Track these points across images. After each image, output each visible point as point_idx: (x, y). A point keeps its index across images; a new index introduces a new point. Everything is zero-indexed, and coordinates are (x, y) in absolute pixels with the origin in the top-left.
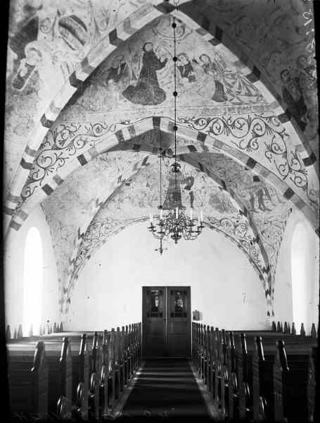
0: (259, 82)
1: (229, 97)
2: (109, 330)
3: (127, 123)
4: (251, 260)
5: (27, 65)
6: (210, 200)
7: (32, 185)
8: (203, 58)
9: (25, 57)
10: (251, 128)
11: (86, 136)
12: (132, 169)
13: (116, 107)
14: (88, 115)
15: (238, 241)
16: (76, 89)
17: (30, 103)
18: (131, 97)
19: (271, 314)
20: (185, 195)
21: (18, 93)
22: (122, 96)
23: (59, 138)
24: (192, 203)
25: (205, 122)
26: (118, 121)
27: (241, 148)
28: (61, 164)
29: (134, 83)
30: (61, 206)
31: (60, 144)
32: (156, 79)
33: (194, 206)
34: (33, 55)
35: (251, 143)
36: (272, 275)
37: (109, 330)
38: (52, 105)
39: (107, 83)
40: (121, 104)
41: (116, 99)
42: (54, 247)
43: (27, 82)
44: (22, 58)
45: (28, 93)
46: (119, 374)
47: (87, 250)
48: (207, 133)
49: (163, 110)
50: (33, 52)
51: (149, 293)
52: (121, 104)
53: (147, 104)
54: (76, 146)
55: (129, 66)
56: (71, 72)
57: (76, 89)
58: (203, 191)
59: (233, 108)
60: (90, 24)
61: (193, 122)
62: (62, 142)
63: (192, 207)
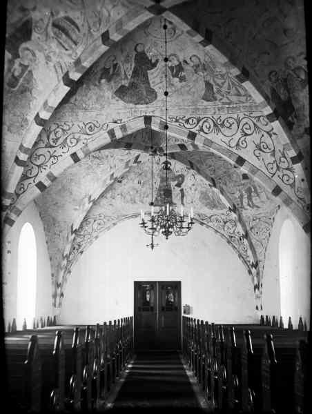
1: (219, 97)
3: (119, 122)
4: (240, 256)
5: (21, 65)
7: (26, 183)
8: (193, 59)
11: (79, 135)
12: (123, 167)
14: (81, 113)
16: (69, 88)
18: (124, 96)
20: (176, 192)
22: (114, 96)
23: (52, 136)
25: (195, 121)
29: (126, 83)
35: (240, 143)
38: (46, 103)
39: (99, 82)
41: (108, 99)
42: (47, 242)
43: (21, 80)
44: (16, 58)
45: (22, 92)
48: (197, 132)
49: (154, 109)
50: (27, 52)
52: (114, 104)
53: (138, 103)
56: (65, 71)
57: (69, 88)
59: (223, 108)
60: (83, 25)
61: (184, 122)
62: (56, 140)
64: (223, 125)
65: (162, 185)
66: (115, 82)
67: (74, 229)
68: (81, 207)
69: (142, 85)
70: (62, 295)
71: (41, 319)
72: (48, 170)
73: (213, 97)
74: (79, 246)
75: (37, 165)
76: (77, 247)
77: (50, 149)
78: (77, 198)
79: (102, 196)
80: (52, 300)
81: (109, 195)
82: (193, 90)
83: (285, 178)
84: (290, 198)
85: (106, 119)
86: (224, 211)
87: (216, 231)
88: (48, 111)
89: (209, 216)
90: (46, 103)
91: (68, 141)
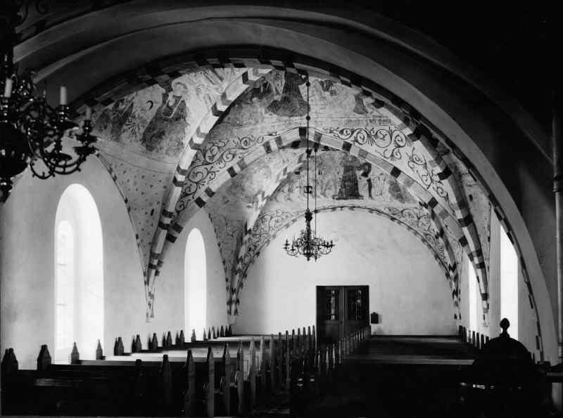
0: (383, 108)
2: (283, 333)
4: (437, 257)
5: (174, 96)
6: (390, 189)
7: (185, 199)
9: (172, 90)
10: (393, 138)
12: (297, 162)
13: (262, 121)
14: (235, 130)
15: (422, 234)
17: (178, 128)
19: (458, 318)
20: (363, 182)
21: (167, 120)
22: (267, 110)
23: (208, 154)
24: (370, 191)
25: (349, 132)
26: (266, 133)
27: (385, 157)
28: (213, 177)
29: (278, 98)
30: (226, 200)
31: (210, 159)
32: (299, 92)
33: (373, 195)
34: (179, 88)
35: (394, 154)
36: (459, 273)
37: (283, 333)
38: (198, 130)
39: (251, 100)
40: (267, 118)
41: (262, 114)
42: (219, 245)
43: (175, 110)
44: (169, 91)
45: (177, 120)
46: (272, 377)
47: (255, 246)
48: (352, 143)
50: (178, 86)
51: (324, 294)
52: (267, 118)
53: (292, 116)
54: (225, 159)
55: (272, 84)
57: (218, 118)
58: (382, 177)
61: (338, 133)
63: (370, 196)
64: (376, 135)
65: (345, 175)
66: (267, 99)
67: (248, 229)
68: (254, 204)
69: (294, 99)
70: (238, 301)
71: (213, 329)
72: (206, 186)
73: (364, 110)
74: (255, 246)
75: (195, 183)
76: (253, 247)
77: (206, 166)
78: (249, 194)
79: (278, 190)
80: (227, 308)
81: (286, 189)
82: (344, 103)
83: (440, 190)
84: (447, 212)
85: (262, 132)
86: (413, 205)
87: (410, 228)
88: (201, 137)
89: (400, 210)
90: (198, 130)
91: (224, 157)
